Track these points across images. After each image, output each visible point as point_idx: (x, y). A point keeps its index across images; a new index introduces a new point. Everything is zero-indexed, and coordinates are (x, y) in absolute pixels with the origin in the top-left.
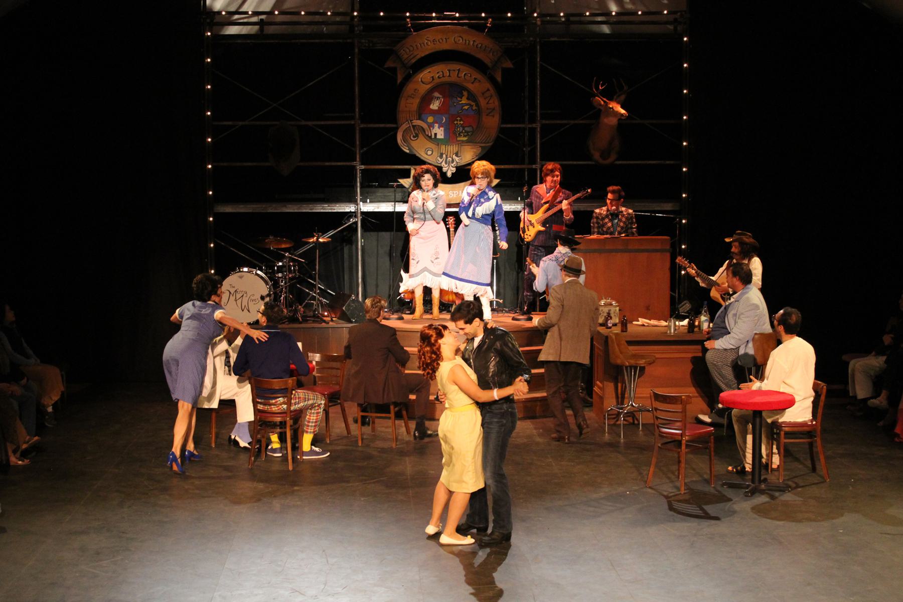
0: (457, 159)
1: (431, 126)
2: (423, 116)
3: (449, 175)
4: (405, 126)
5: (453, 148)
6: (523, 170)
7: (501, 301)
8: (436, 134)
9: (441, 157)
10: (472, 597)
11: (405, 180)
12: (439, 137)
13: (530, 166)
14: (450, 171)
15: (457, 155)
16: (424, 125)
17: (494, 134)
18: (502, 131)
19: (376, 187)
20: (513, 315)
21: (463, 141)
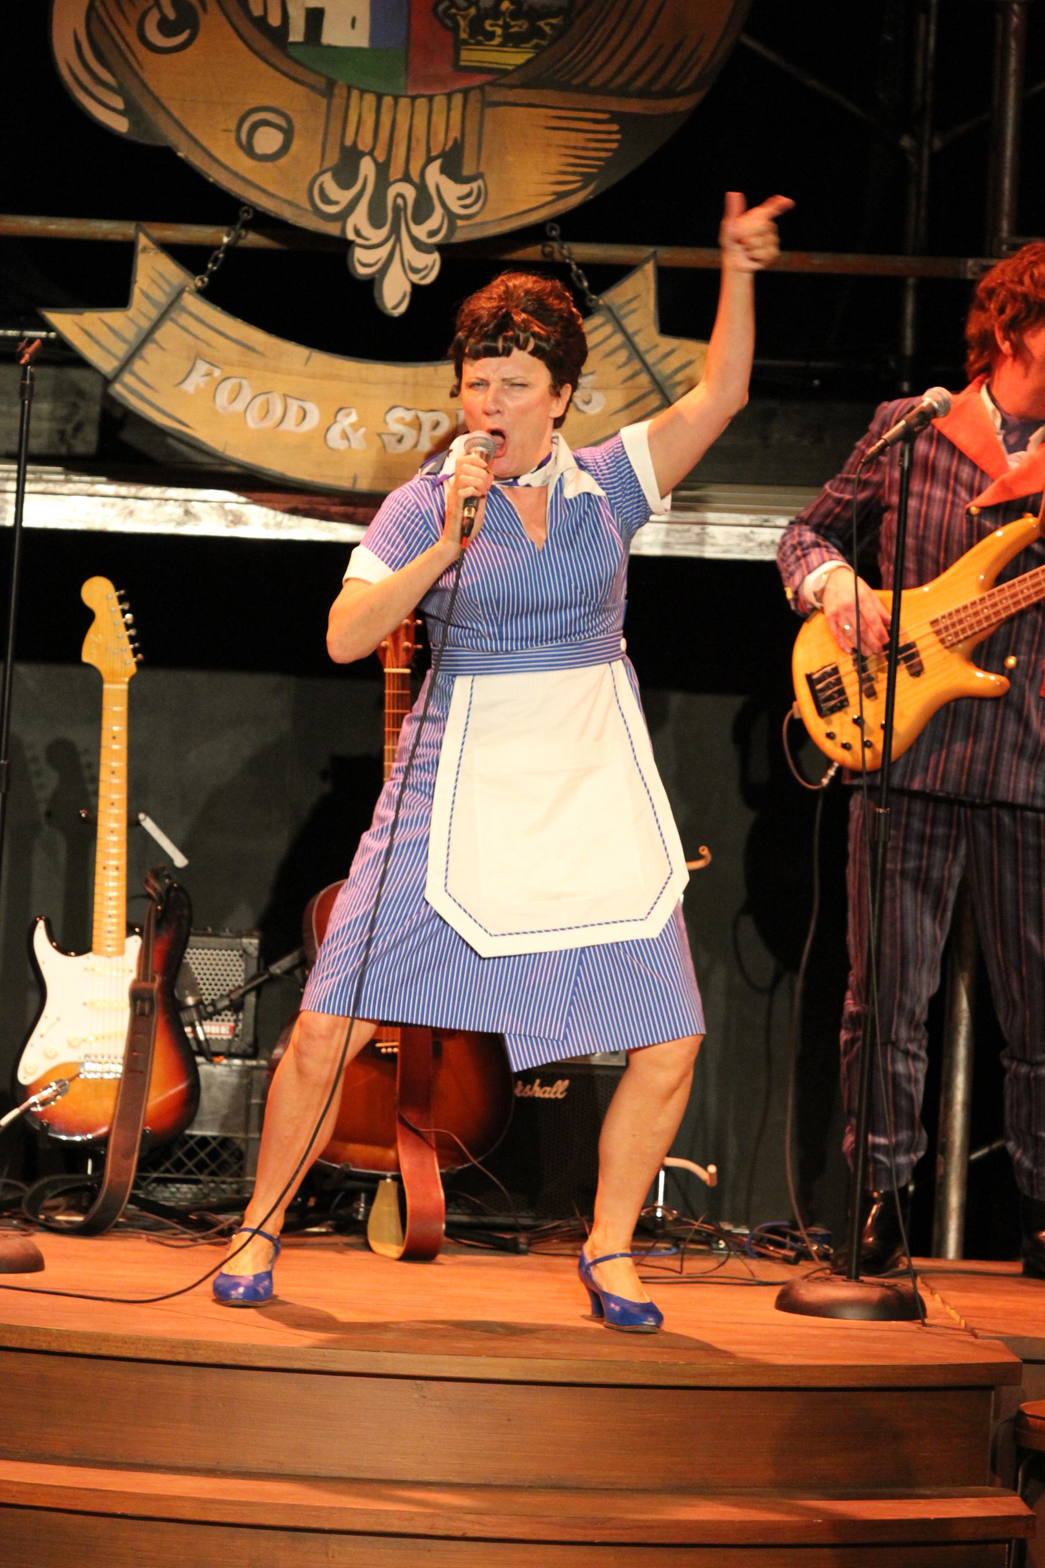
0: (452, 192)
3: (394, 296)
5: (440, 119)
6: (891, 288)
7: (707, 1173)
9: (346, 172)
11: (94, 319)
12: (336, 34)
13: (940, 267)
14: (398, 272)
15: (452, 169)
20: (781, 1273)
21: (498, 76)
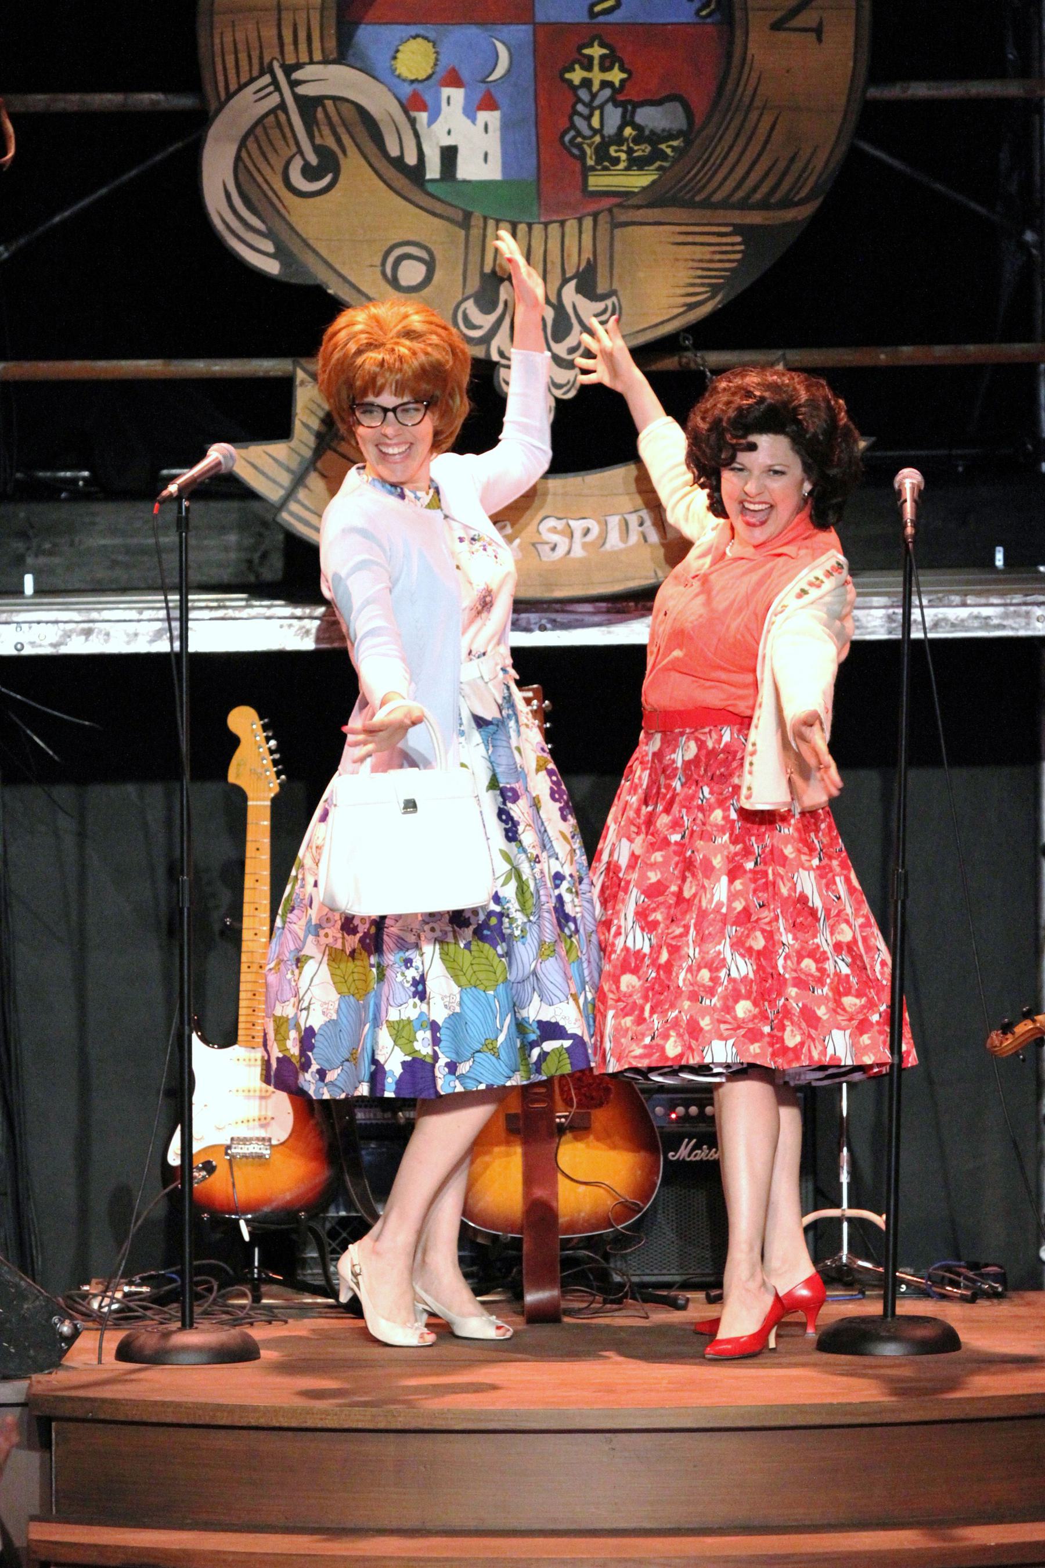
1: (414, 103)
2: (366, 35)
4: (247, 106)
8: (449, 155)
10: (483, 760)
11: (257, 452)
16: (379, 102)
17: (820, 140)
18: (871, 120)
19: (80, 495)
